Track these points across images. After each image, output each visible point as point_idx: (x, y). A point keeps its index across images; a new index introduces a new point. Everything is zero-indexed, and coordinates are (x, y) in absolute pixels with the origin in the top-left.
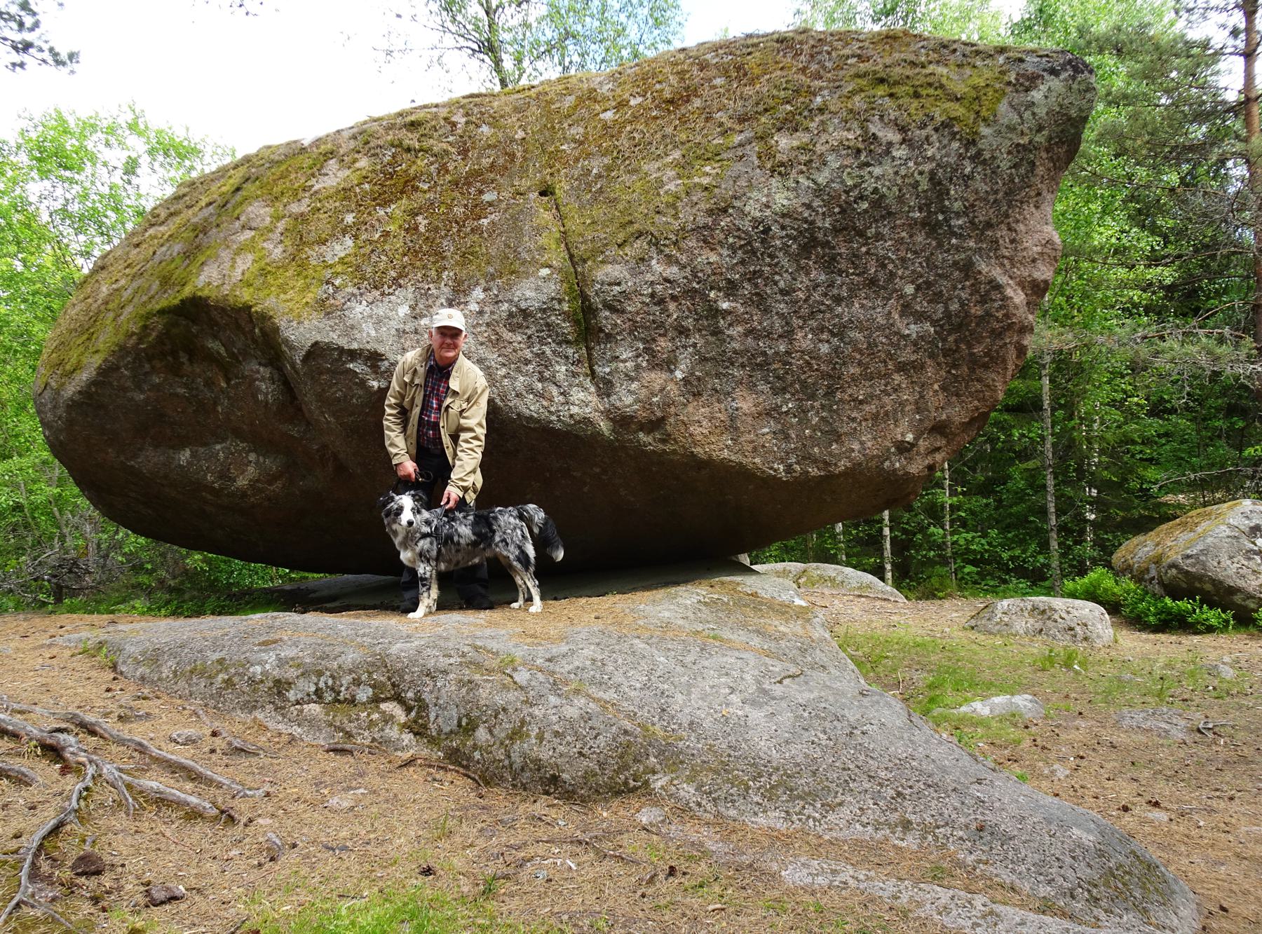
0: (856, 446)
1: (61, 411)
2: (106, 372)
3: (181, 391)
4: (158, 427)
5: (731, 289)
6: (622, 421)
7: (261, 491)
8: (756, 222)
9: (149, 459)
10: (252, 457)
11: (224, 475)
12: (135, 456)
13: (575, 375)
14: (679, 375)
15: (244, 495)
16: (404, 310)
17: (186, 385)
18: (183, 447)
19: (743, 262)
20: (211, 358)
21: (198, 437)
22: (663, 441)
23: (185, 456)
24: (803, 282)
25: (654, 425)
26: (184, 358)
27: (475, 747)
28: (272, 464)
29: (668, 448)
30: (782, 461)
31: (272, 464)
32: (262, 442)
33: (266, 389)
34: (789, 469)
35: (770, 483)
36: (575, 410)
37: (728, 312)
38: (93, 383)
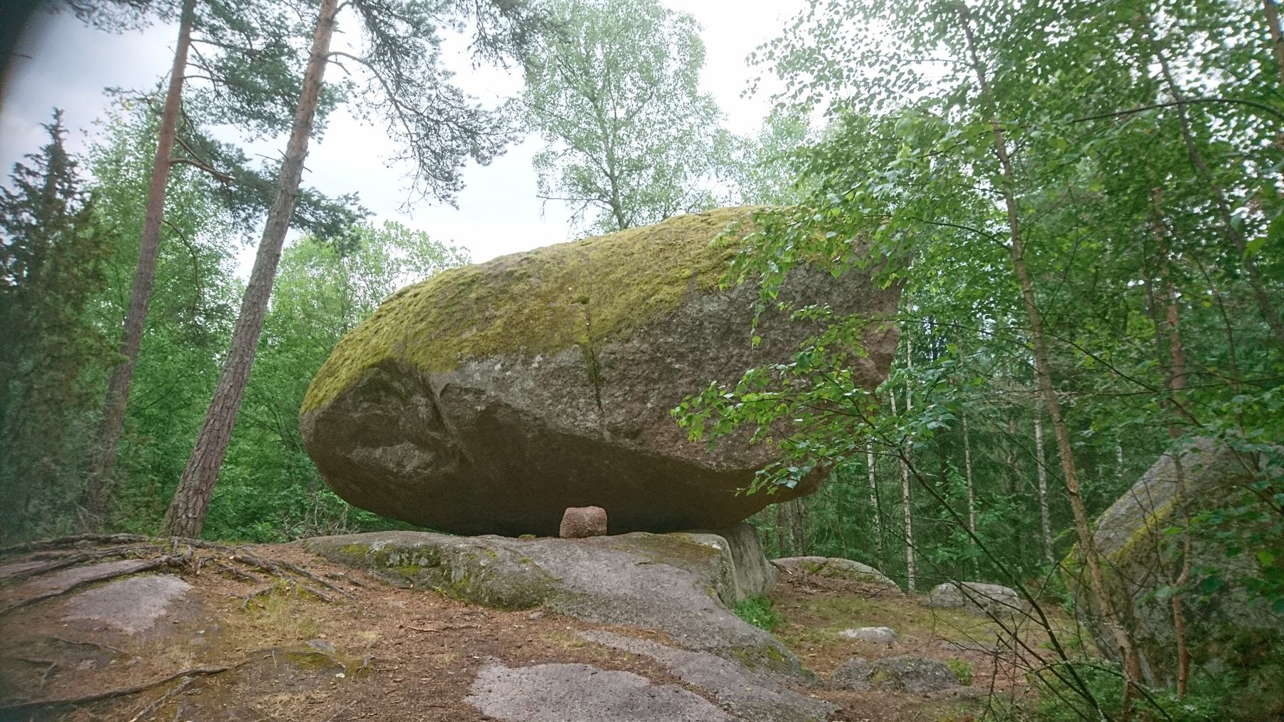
0: (762, 452)
1: (313, 424)
2: (341, 398)
3: (379, 412)
4: (365, 434)
5: (681, 357)
6: (615, 431)
7: (419, 474)
8: (694, 320)
9: (358, 453)
10: (417, 452)
11: (400, 464)
12: (350, 452)
13: (590, 404)
14: (649, 405)
15: (411, 477)
16: (498, 367)
17: (381, 409)
18: (378, 446)
19: (687, 342)
20: (397, 394)
21: (391, 440)
22: (641, 444)
23: (378, 452)
24: (723, 355)
25: (634, 434)
26: (382, 393)
27: (139, 176)
28: (428, 457)
29: (644, 448)
30: (715, 459)
31: (428, 457)
32: (421, 443)
33: (424, 412)
34: (719, 465)
35: (709, 472)
36: (589, 424)
37: (679, 370)
38: (332, 407)
